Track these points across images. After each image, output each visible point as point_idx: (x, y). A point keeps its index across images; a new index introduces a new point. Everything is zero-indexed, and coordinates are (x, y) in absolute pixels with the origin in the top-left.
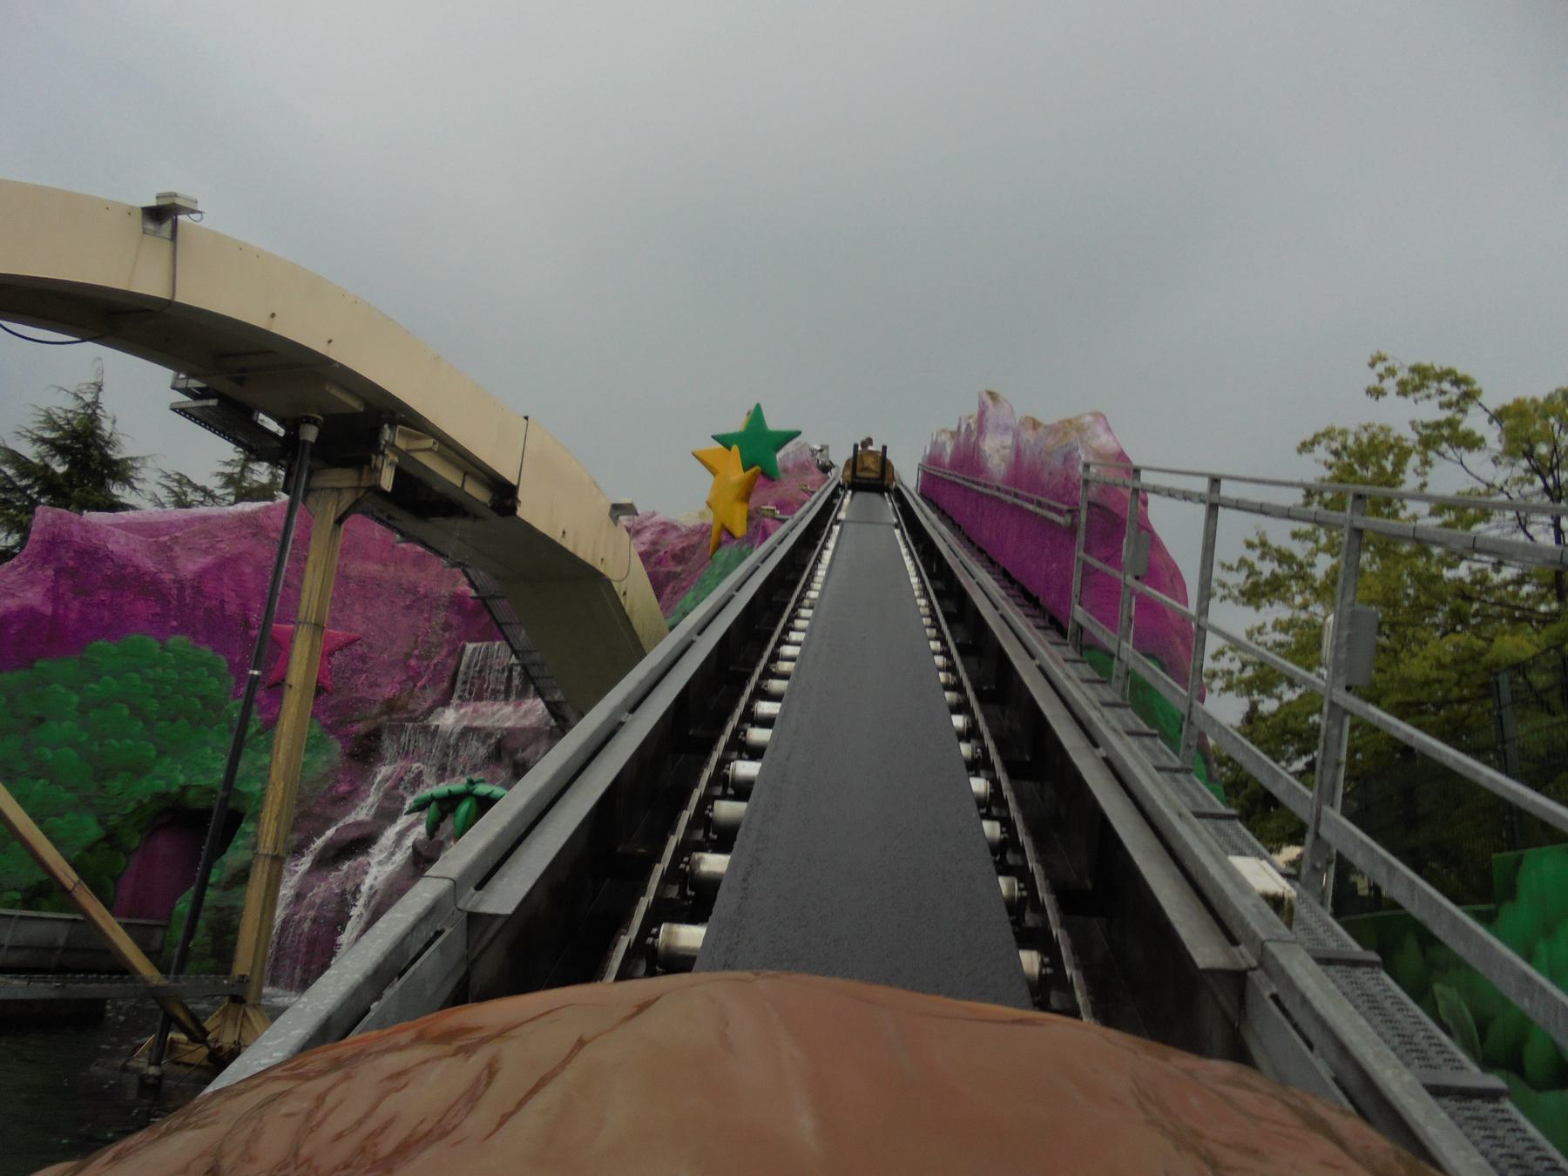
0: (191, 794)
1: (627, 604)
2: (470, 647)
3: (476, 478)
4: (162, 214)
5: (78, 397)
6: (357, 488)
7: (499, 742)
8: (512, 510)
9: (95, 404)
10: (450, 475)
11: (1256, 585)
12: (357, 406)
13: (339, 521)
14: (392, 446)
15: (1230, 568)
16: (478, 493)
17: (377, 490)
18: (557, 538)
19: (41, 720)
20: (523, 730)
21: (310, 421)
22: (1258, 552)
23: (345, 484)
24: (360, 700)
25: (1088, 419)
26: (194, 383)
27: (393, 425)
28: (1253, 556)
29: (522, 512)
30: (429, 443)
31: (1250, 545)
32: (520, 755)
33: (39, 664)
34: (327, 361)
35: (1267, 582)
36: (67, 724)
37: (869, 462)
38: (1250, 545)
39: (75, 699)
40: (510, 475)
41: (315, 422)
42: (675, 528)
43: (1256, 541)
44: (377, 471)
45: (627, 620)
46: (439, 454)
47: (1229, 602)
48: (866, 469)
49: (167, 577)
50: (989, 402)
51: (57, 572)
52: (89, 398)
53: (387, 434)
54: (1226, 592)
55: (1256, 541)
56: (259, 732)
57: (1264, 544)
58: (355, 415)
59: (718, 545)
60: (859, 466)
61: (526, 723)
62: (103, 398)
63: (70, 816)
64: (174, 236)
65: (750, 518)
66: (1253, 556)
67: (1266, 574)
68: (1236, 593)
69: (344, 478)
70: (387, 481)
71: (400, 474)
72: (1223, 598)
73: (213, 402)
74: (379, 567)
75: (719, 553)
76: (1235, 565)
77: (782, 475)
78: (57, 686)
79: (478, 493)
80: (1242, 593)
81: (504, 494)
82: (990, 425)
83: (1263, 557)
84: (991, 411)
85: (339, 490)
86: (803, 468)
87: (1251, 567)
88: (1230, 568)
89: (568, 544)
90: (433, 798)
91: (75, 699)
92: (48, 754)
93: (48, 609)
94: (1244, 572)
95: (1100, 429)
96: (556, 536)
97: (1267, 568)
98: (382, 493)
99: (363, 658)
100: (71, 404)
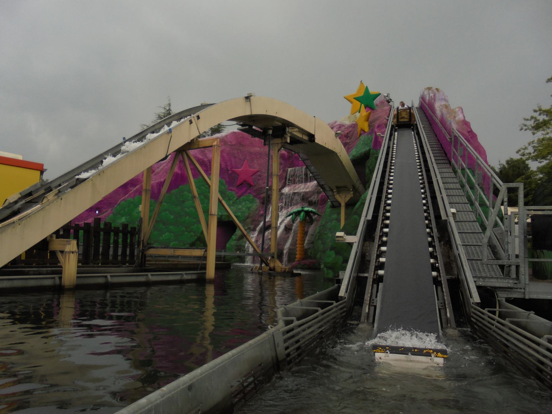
0: (223, 217)
1: (341, 158)
2: (290, 169)
3: (305, 134)
4: (248, 98)
5: (165, 109)
6: (282, 143)
7: (303, 196)
8: (314, 141)
9: (170, 110)
10: (300, 135)
11: (538, 124)
12: (280, 124)
13: (278, 151)
14: (289, 132)
15: (528, 120)
16: (305, 138)
17: (286, 143)
18: (324, 145)
19: (184, 201)
20: (309, 192)
21: (270, 129)
22: (538, 113)
23: (279, 142)
24: (261, 188)
25: (457, 109)
26: (241, 123)
27: (288, 127)
28: (536, 115)
29: (316, 141)
30: (296, 129)
31: (535, 111)
32: (310, 199)
33: (181, 187)
34: (276, 117)
35: (542, 123)
36: (190, 202)
37: (404, 114)
38: (535, 111)
39: (190, 195)
40: (313, 133)
41: (271, 129)
42: (343, 126)
43: (537, 109)
44: (286, 138)
45: (341, 162)
46: (299, 131)
47: (528, 130)
48: (403, 118)
49: (206, 159)
50: (436, 92)
51: (180, 162)
52: (168, 108)
53: (287, 129)
54: (526, 128)
55: (537, 109)
56: (237, 199)
57: (540, 110)
58: (280, 126)
59: (361, 135)
60: (400, 117)
61: (308, 190)
62: (171, 108)
63: (195, 225)
64: (250, 101)
65: (369, 126)
66: (536, 115)
67: (541, 120)
68: (530, 128)
69: (278, 141)
70: (288, 141)
71: (291, 137)
72: (526, 130)
73: (247, 127)
74: (259, 149)
75: (361, 137)
76: (529, 118)
77: (376, 108)
78: (186, 192)
79: (305, 138)
80: (533, 127)
81: (312, 137)
82: (437, 99)
83: (540, 115)
84: (437, 95)
85: (278, 144)
86: (382, 103)
87: (535, 118)
88: (528, 120)
89: (327, 146)
90: (294, 212)
91: (190, 195)
92: (187, 209)
93: (179, 172)
94: (533, 121)
95: (460, 113)
96: (324, 145)
97: (542, 118)
98: (288, 143)
99: (260, 176)
100: (163, 111)
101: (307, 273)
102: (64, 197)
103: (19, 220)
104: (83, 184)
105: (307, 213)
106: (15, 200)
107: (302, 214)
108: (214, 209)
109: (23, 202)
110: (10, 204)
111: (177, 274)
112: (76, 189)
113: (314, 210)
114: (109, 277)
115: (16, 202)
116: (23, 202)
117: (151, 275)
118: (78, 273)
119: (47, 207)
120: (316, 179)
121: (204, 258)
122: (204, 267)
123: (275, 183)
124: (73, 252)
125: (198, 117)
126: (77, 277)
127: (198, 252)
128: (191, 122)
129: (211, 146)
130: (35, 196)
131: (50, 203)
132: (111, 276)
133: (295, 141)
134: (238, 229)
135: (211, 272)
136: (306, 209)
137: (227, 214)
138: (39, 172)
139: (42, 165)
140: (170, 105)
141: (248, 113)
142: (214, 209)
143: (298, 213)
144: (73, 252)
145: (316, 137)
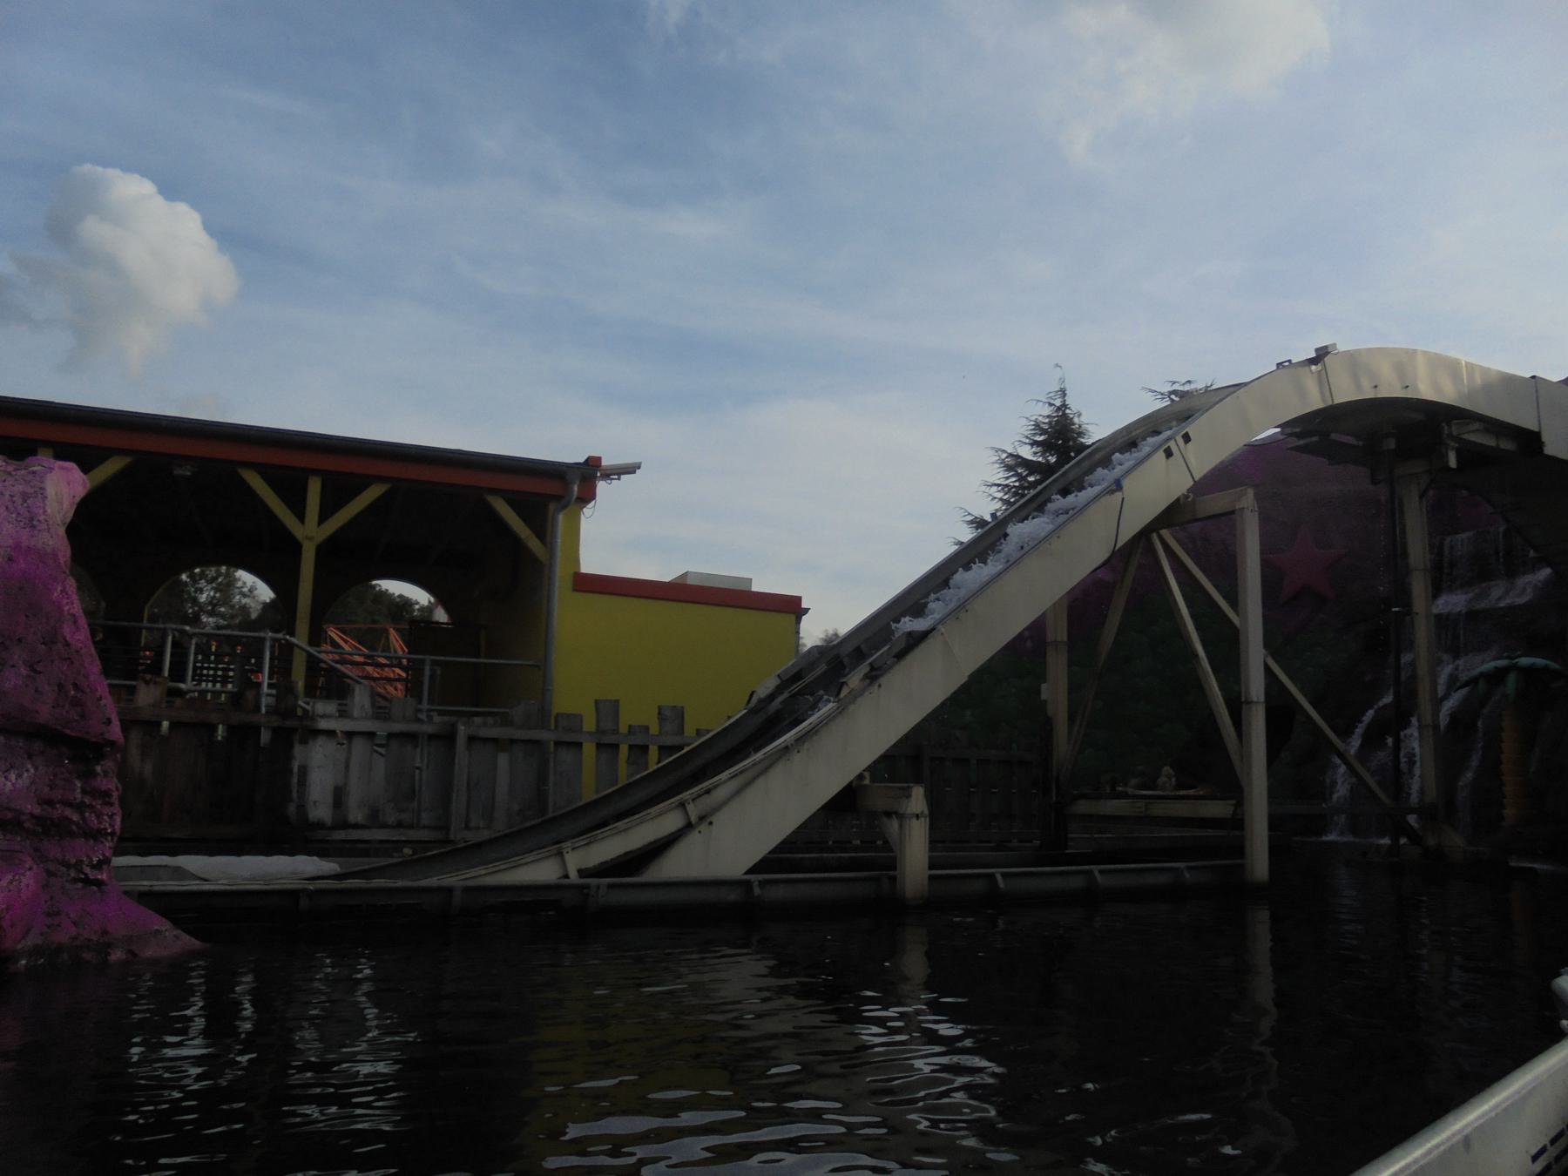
10: (1489, 441)
14: (1450, 435)
30: (1477, 425)
40: (1531, 425)
52: (1058, 403)
70: (1453, 463)
73: (1315, 439)
79: (1507, 445)
100: (1047, 411)
101: (1181, 1118)
102: (883, 680)
103: (797, 740)
104: (923, 646)
105: (1529, 671)
106: (768, 691)
107: (1511, 679)
108: (1256, 687)
109: (786, 695)
110: (760, 701)
111: (1163, 869)
112: (909, 658)
113: (1553, 665)
114: (999, 877)
115: (772, 697)
116: (786, 695)
117: (1101, 872)
118: (930, 868)
119: (852, 708)
120: (1549, 565)
121: (1237, 823)
122: (1238, 849)
123: (1419, 587)
124: (918, 817)
125: (1187, 438)
126: (931, 877)
127: (1218, 809)
128: (1169, 453)
129: (1233, 512)
130: (808, 679)
131: (855, 696)
132: (1004, 875)
133: (1473, 457)
134: (296, 650)
135: (1259, 863)
136: (1525, 661)
137: (62, 487)
138: (793, 617)
139: (799, 599)
140: (1063, 393)
141: (1315, 402)
142: (1256, 687)
143: (1497, 677)
144: (918, 817)
145: (1544, 438)
